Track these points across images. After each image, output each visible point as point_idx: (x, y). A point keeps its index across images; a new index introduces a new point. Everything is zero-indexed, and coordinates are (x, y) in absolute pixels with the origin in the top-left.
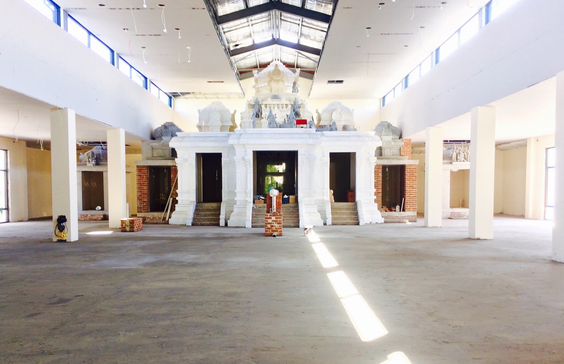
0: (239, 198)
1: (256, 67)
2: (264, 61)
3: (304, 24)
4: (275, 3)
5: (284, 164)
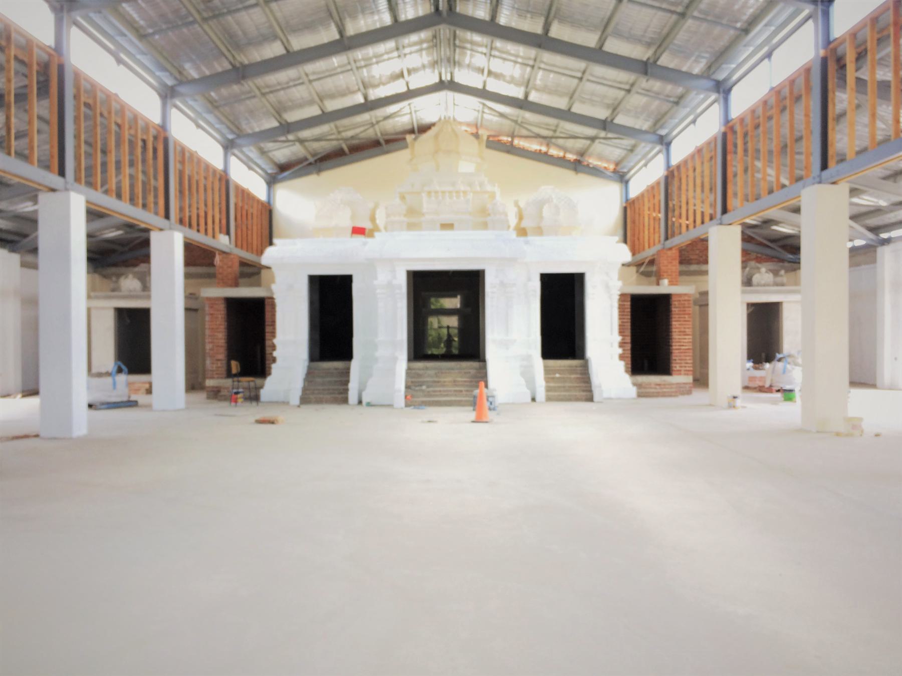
0: (896, 213)
1: (412, 131)
2: (428, 119)
3: (494, 53)
4: (445, 16)
5: (459, 297)
